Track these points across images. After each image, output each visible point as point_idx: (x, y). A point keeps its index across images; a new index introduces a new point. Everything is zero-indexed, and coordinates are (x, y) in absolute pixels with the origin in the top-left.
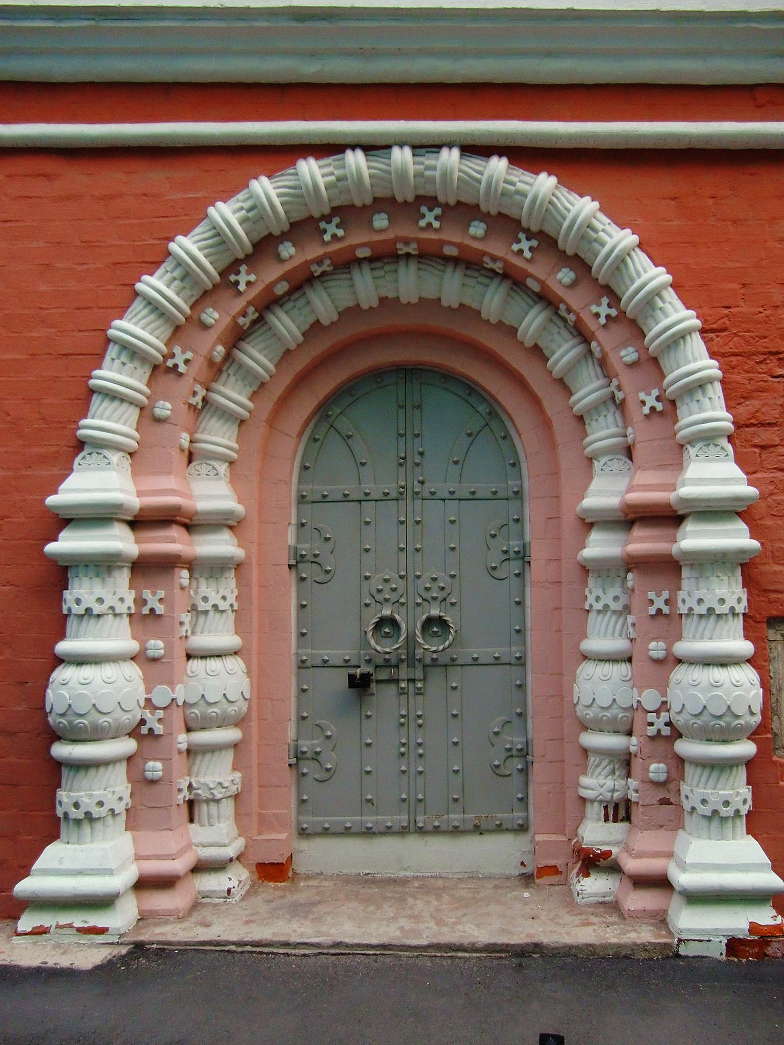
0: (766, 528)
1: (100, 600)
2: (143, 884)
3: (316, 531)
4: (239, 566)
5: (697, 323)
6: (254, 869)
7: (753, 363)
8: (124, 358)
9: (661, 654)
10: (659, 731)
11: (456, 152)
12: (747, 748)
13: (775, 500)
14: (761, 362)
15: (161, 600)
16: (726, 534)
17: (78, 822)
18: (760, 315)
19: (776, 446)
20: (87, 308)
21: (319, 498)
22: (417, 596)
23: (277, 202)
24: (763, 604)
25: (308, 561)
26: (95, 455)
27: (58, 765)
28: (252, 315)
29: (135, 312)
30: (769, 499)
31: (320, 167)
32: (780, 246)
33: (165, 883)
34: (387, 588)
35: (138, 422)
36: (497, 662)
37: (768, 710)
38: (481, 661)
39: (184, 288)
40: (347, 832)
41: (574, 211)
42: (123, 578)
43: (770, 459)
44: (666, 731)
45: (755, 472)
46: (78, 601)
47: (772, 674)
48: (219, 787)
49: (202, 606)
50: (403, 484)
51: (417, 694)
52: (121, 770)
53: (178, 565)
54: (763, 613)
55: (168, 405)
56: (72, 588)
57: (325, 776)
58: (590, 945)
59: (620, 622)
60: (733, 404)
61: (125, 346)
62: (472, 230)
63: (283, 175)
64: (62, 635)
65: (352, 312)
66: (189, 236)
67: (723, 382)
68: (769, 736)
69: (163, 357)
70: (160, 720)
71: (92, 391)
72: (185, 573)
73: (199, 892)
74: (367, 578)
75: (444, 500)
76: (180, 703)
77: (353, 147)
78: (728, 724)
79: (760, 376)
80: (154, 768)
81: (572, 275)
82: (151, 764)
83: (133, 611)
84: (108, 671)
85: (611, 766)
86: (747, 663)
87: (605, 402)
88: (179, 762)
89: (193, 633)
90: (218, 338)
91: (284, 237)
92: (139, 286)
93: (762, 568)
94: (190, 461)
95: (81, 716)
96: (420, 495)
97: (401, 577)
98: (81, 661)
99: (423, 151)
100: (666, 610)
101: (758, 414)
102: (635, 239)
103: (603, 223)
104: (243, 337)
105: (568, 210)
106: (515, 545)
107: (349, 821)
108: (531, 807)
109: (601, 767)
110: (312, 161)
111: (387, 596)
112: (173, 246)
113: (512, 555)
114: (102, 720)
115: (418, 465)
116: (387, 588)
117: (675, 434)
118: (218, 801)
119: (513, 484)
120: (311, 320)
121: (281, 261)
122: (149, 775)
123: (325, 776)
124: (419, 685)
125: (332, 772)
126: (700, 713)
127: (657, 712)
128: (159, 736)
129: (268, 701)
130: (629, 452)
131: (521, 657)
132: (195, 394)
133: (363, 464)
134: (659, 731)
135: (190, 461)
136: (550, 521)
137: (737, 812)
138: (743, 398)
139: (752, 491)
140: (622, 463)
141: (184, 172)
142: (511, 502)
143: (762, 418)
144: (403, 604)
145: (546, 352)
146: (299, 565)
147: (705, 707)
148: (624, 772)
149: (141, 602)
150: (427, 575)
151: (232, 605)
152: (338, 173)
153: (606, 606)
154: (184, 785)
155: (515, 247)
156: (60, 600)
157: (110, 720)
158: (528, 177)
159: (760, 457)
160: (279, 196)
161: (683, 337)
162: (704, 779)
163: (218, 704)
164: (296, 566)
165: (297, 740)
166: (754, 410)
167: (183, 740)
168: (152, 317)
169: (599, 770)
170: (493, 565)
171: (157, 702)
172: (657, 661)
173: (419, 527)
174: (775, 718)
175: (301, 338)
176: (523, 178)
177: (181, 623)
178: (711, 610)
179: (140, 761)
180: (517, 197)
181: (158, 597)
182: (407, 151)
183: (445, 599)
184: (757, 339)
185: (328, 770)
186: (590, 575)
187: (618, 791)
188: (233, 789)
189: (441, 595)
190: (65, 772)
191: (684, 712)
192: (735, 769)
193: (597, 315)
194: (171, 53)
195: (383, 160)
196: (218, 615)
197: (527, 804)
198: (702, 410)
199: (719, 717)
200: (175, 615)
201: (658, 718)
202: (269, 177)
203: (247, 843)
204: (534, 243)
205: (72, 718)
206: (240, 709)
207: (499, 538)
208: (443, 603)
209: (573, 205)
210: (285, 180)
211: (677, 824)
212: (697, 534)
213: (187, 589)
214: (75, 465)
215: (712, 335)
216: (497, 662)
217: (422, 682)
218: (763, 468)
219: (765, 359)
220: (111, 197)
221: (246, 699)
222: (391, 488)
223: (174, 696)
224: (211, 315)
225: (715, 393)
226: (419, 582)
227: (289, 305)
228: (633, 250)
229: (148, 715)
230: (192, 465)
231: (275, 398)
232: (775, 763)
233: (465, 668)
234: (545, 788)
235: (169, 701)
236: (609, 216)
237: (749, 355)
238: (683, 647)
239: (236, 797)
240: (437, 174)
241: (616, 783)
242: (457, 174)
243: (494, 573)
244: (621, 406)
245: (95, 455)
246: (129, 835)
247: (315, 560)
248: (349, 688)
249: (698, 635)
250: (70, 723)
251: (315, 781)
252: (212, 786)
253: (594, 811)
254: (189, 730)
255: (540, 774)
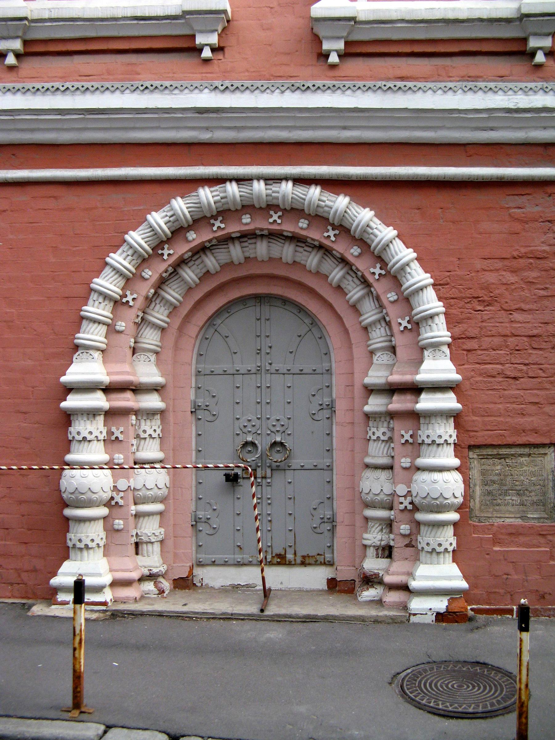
0: (469, 396)
1: (91, 433)
2: (115, 584)
3: (207, 392)
4: (162, 412)
5: (431, 281)
6: (172, 582)
7: (463, 303)
8: (101, 300)
9: (408, 465)
10: (406, 507)
11: (290, 184)
12: (454, 516)
13: (474, 381)
14: (468, 303)
15: (121, 432)
16: (443, 400)
17: (81, 549)
18: (468, 276)
19: (476, 350)
20: (78, 271)
21: (208, 372)
22: (267, 430)
23: (186, 211)
24: (465, 438)
25: (202, 409)
26: (85, 354)
27: (67, 519)
28: (171, 270)
29: (106, 275)
30: (471, 380)
31: (211, 192)
32: (480, 237)
33: (127, 583)
34: (249, 424)
35: (106, 334)
36: (315, 468)
37: (468, 495)
38: (305, 467)
39: (133, 259)
40: (226, 564)
41: (359, 217)
42: (100, 419)
43: (472, 357)
44: (410, 507)
45: (463, 365)
46: (79, 433)
47: (470, 477)
48: (153, 535)
49: (143, 435)
50: (259, 365)
51: (268, 486)
52: (100, 525)
53: (131, 413)
54: (466, 443)
55: (123, 324)
56: (75, 426)
57: (211, 532)
58: (361, 616)
59: (387, 446)
60: (451, 326)
61: (100, 293)
62: (300, 225)
63: (189, 196)
64: (68, 451)
65: (229, 265)
66: (136, 231)
67: (445, 314)
68: (467, 510)
69: (120, 296)
70: (122, 498)
71: (83, 318)
72: (134, 417)
73: (143, 591)
74: (238, 419)
75: (284, 374)
76: (132, 489)
77: (231, 180)
78: (441, 503)
79: (467, 310)
80: (119, 523)
81: (359, 250)
82: (117, 521)
83: (106, 438)
84: (446, 475)
85: (380, 527)
86: (456, 471)
87: (379, 321)
88: (131, 520)
89: (138, 450)
90: (152, 286)
91: (190, 228)
92: (108, 260)
93: (466, 418)
94: (133, 354)
95: (83, 494)
96: (269, 371)
97: (258, 419)
98: (82, 466)
99: (271, 182)
100: (411, 440)
101: (466, 332)
102: (395, 232)
103: (377, 224)
104: (164, 281)
105: (356, 217)
106: (327, 401)
107: (228, 557)
108: (335, 552)
109: (375, 527)
110: (207, 189)
111: (250, 430)
112: (127, 237)
113: (325, 406)
114: (94, 496)
115: (268, 353)
116: (249, 424)
117: (419, 342)
118: (152, 543)
119: (326, 365)
120: (204, 271)
121: (188, 241)
122: (116, 527)
123: (211, 532)
124: (269, 481)
125: (216, 530)
126: (426, 497)
127: (405, 497)
128: (121, 506)
129: (179, 489)
130: (393, 350)
131: (329, 466)
132: (138, 316)
133: (235, 353)
134: (406, 507)
135: (133, 354)
136: (347, 387)
137: (446, 550)
138: (457, 323)
139: (458, 377)
140: (389, 356)
141: (133, 194)
142: (324, 375)
143: (468, 334)
144: (259, 434)
145: (345, 290)
146: (197, 411)
147: (428, 493)
148: (388, 530)
149: (110, 433)
150: (273, 418)
151: (159, 435)
152: (222, 195)
153: (378, 437)
154: (134, 534)
155: (326, 234)
156: (66, 432)
157: (97, 497)
158: (332, 197)
159: (467, 356)
160: (187, 208)
161: (422, 289)
162: (428, 533)
163: (153, 490)
164: (195, 412)
165: (196, 512)
166: (463, 330)
167: (133, 509)
168: (116, 276)
169: (374, 529)
170: (314, 412)
171: (120, 488)
172: (405, 469)
173: (269, 390)
174: (472, 500)
175: (197, 281)
176: (330, 198)
177: (132, 445)
178: (434, 442)
179: (111, 519)
180: (326, 209)
181: (120, 430)
182: (262, 183)
183: (284, 432)
184: (466, 290)
185: (214, 528)
186: (370, 419)
187: (384, 540)
188: (161, 538)
189: (282, 429)
190: (71, 524)
191: (418, 496)
192: (446, 527)
193: (374, 273)
194: (32, 130)
195: (248, 187)
196: (151, 440)
197: (333, 550)
198: (432, 330)
199: (436, 499)
200: (129, 441)
201: (405, 500)
202: (182, 198)
203: (168, 567)
204: (337, 232)
205: (78, 495)
206: (164, 493)
207: (317, 396)
208: (283, 434)
209: (359, 214)
210: (191, 200)
211: (416, 559)
212: (427, 400)
213: (134, 426)
214: (74, 359)
215: (440, 287)
216: (315, 468)
217: (270, 479)
218: (469, 363)
219: (471, 301)
220: (91, 209)
221: (167, 487)
222: (252, 367)
223: (129, 485)
224: (147, 273)
225: (440, 321)
226: (269, 421)
227: (190, 264)
228: (394, 239)
229: (115, 494)
230: (135, 356)
231: (183, 316)
232: (470, 524)
233: (295, 471)
234: (344, 540)
235: (126, 487)
236: (380, 220)
237: (461, 298)
238: (422, 461)
239: (162, 542)
240: (280, 196)
241: (383, 536)
242: (291, 196)
243: (314, 417)
244: (388, 324)
245: (85, 354)
246: (105, 558)
247: (207, 408)
248: (226, 481)
249: (427, 455)
250: (77, 497)
251: (206, 535)
252: (149, 534)
253: (371, 552)
254: (135, 504)
255: (341, 531)
